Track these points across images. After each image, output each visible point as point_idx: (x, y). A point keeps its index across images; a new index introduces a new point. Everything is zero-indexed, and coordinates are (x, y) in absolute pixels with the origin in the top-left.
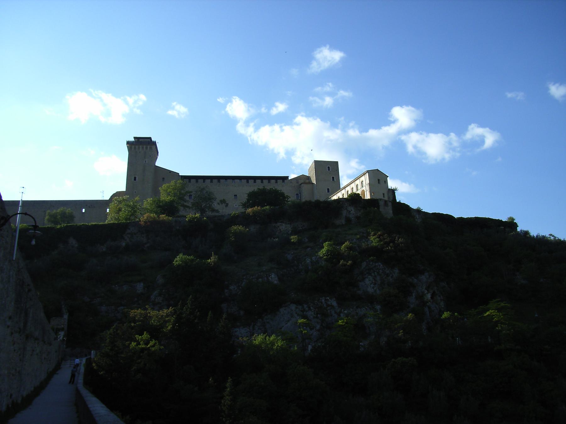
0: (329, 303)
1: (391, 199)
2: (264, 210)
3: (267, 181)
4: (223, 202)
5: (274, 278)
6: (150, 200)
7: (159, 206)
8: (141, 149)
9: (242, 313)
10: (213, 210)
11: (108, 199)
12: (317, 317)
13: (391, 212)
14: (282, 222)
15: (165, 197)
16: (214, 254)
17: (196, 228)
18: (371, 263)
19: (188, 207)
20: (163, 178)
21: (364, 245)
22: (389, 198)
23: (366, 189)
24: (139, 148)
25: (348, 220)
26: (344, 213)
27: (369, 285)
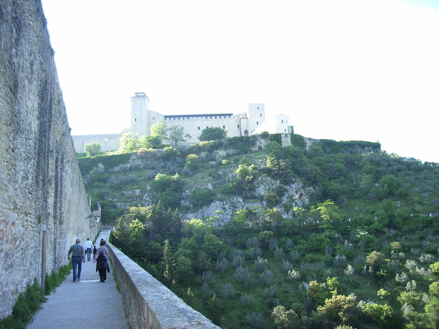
0: (238, 200)
1: (290, 133)
2: (209, 143)
4: (188, 135)
5: (210, 187)
7: (149, 141)
9: (192, 205)
10: (183, 140)
12: (230, 208)
15: (154, 135)
17: (170, 156)
19: (167, 138)
22: (289, 132)
24: (137, 100)
25: (260, 148)
26: (258, 143)
27: (261, 191)
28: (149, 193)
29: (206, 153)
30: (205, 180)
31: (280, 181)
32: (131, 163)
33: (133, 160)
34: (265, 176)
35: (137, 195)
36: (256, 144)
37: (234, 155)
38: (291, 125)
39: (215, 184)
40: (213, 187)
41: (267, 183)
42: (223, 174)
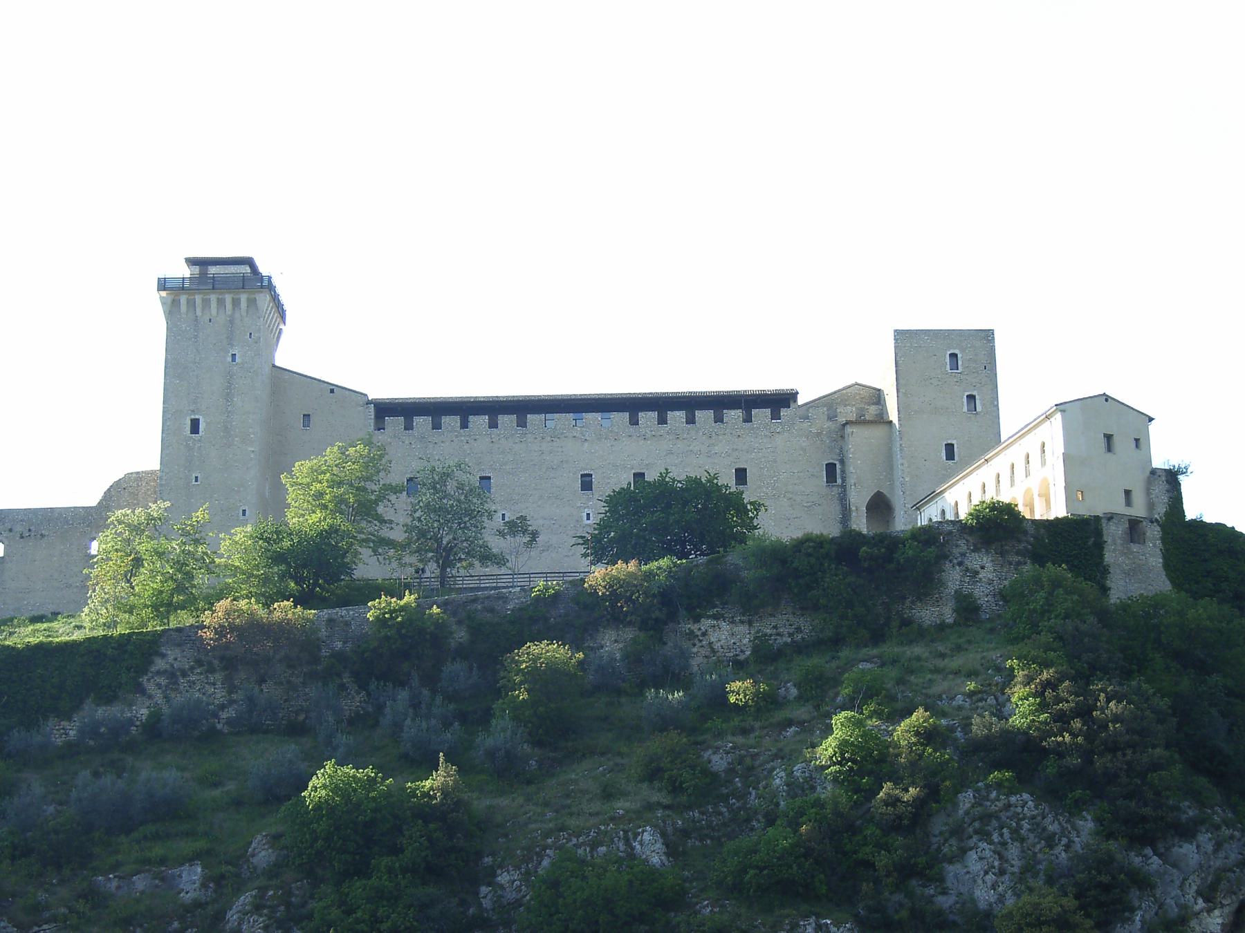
1: (1161, 510)
2: (649, 575)
3: (710, 414)
4: (517, 527)
5: (650, 847)
6: (243, 533)
7: (278, 558)
8: (214, 305)
10: (487, 557)
11: (144, 453)
13: (1156, 561)
14: (716, 617)
15: (304, 518)
16: (446, 761)
17: (403, 654)
18: (994, 794)
19: (390, 543)
20: (307, 416)
21: (980, 725)
22: (1151, 506)
23: (1054, 474)
24: (206, 303)
25: (968, 609)
26: (953, 578)
28: (263, 890)
29: (629, 634)
30: (621, 806)
31: (1098, 820)
32: (159, 697)
33: (172, 675)
34: (999, 785)
35: (187, 897)
36: (942, 583)
37: (800, 649)
38: (1160, 459)
39: (685, 833)
40: (672, 850)
41: (1015, 832)
42: (731, 771)
